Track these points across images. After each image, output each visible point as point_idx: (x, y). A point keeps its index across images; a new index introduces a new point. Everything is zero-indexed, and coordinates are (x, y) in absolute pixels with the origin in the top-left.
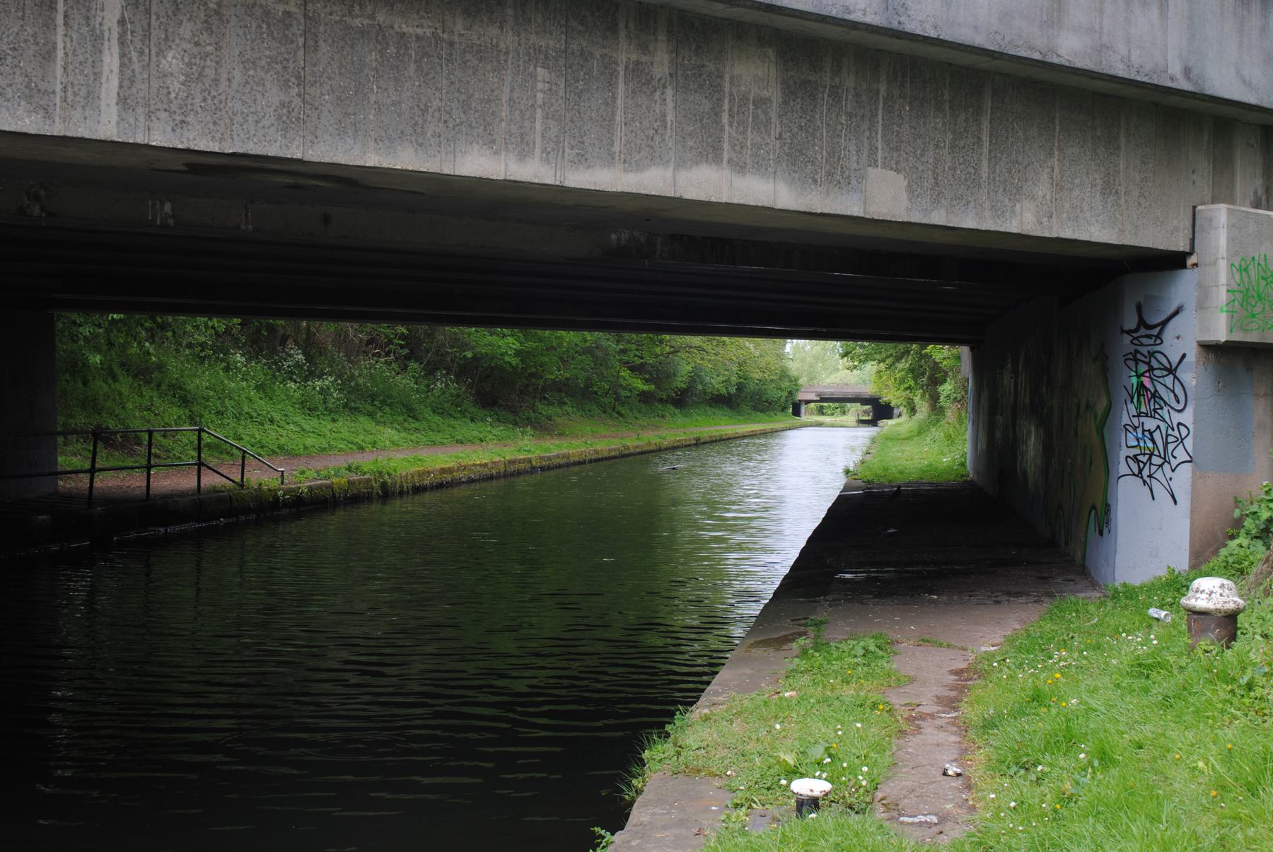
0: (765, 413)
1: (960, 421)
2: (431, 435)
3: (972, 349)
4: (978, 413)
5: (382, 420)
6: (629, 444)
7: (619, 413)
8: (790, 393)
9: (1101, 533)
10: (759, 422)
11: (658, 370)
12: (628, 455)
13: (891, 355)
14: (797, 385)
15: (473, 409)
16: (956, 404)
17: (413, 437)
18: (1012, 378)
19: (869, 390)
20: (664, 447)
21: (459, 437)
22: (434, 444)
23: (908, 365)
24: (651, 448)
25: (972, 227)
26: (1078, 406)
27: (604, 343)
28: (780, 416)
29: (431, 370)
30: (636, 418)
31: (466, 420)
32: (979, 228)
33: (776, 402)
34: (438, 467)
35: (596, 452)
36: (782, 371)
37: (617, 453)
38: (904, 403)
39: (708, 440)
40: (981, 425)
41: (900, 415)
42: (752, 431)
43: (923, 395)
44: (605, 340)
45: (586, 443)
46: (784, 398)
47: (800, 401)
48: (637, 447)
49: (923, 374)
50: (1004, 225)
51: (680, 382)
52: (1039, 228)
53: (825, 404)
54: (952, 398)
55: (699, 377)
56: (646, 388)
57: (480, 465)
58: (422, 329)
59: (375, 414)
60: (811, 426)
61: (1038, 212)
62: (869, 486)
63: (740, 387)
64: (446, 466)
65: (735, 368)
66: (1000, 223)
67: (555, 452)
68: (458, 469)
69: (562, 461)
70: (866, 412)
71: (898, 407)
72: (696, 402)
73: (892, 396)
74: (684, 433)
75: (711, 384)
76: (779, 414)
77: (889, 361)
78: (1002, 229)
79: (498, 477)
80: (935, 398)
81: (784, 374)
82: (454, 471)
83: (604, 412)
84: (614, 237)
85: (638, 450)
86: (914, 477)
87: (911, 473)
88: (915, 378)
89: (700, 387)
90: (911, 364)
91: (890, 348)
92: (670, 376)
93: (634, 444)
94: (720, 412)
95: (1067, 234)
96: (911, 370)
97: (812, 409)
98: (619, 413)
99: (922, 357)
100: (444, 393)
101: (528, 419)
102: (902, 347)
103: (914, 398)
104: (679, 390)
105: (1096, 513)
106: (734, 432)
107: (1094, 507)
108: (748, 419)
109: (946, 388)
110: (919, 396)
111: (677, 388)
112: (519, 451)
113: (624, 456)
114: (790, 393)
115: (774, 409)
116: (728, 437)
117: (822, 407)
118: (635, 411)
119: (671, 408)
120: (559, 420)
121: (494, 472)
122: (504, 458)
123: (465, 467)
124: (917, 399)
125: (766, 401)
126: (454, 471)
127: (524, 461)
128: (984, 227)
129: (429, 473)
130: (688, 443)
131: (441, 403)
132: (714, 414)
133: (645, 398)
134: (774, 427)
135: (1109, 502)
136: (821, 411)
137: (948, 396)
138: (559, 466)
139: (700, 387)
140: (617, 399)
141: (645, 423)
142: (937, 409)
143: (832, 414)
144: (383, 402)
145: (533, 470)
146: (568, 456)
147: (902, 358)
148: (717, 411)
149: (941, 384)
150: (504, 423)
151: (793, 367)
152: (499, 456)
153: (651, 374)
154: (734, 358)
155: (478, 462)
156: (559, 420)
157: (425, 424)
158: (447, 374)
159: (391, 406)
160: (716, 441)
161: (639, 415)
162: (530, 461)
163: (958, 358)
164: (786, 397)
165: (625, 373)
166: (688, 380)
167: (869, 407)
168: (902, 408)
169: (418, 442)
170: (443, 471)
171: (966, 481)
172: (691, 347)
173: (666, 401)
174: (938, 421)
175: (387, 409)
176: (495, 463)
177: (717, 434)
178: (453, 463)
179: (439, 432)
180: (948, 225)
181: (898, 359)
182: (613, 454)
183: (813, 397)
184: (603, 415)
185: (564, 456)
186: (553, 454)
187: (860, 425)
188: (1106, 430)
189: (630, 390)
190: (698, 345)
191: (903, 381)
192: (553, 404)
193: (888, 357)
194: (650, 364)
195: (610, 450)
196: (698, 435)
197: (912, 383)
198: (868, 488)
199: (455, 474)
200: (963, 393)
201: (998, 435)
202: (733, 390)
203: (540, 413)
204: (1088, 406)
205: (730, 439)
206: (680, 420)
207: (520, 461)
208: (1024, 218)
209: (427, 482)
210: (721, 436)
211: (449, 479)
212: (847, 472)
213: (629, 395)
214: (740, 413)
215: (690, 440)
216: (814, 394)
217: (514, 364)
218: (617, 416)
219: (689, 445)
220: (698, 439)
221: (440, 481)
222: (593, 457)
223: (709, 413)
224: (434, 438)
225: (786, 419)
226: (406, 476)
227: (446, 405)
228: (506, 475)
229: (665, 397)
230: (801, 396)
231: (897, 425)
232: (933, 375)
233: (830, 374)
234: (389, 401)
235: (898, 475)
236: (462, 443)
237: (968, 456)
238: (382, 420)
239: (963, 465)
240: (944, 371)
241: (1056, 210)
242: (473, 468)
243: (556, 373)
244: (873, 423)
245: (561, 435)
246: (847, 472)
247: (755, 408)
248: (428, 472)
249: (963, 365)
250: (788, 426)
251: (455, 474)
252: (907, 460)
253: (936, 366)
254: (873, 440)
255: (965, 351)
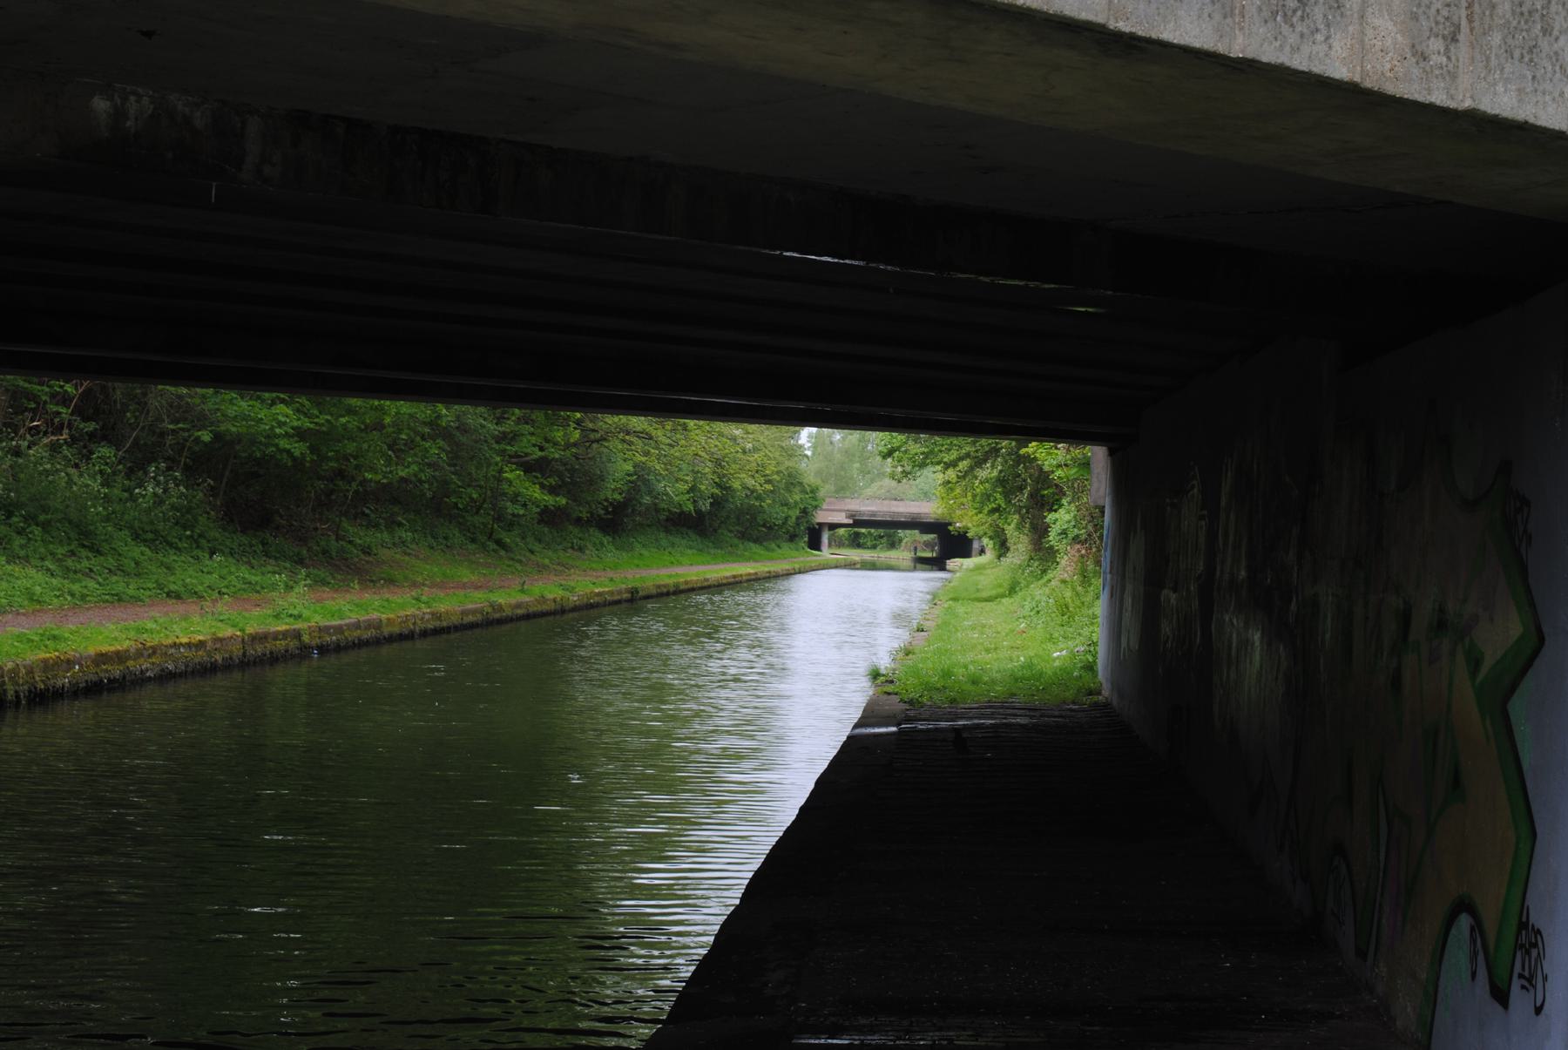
0: (761, 544)
1: (1085, 579)
2: (118, 584)
3: (1112, 453)
4: (1123, 577)
5: (22, 553)
6: (501, 601)
7: (499, 543)
8: (804, 511)
9: (1501, 996)
10: (748, 560)
11: (572, 471)
12: (500, 622)
13: (968, 455)
14: (815, 499)
15: (215, 534)
16: (1078, 546)
17: (76, 587)
18: (1202, 518)
19: (931, 509)
20: (571, 605)
21: (173, 587)
22: (120, 600)
23: (995, 473)
24: (545, 608)
25: (1197, 44)
26: (1405, 619)
27: (471, 420)
28: (786, 549)
29: (136, 464)
30: (532, 552)
31: (200, 553)
32: (1221, 48)
33: (781, 527)
34: (92, 651)
35: (436, 616)
36: (790, 475)
37: (479, 617)
38: (990, 533)
39: (654, 592)
40: (1128, 601)
41: (982, 551)
42: (734, 577)
43: (1019, 527)
44: (478, 418)
45: (417, 599)
46: (794, 519)
47: (820, 524)
48: (518, 606)
49: (1021, 489)
50: (1306, 49)
51: (612, 490)
52: (1416, 72)
53: (863, 530)
54: (1070, 536)
55: (646, 482)
56: (549, 500)
57: (189, 645)
58: (119, 390)
59: (10, 541)
60: (836, 567)
61: (1415, 17)
62: (912, 713)
63: (717, 503)
64: (112, 649)
65: (707, 469)
66: (1293, 39)
67: (353, 617)
68: (139, 654)
69: (367, 635)
70: (928, 545)
71: (980, 538)
72: (641, 525)
73: (968, 521)
74: (611, 580)
75: (667, 494)
76: (785, 545)
77: (963, 465)
78: (1299, 63)
79: (228, 666)
80: (1040, 532)
81: (793, 480)
82: (128, 658)
83: (473, 541)
84: (100, 105)
85: (520, 612)
86: (992, 707)
87: (993, 682)
88: (1007, 495)
89: (647, 500)
90: (1001, 471)
91: (962, 446)
92: (595, 480)
93: (513, 601)
94: (684, 542)
95: (1503, 102)
96: (1001, 481)
97: (841, 538)
98: (499, 543)
99: (1021, 460)
100: (161, 502)
101: (325, 552)
102: (985, 443)
103: (1006, 527)
104: (611, 504)
105: (1477, 927)
106: (701, 578)
107: (1464, 906)
108: (730, 553)
109: (1062, 518)
110: (1013, 526)
111: (606, 500)
112: (277, 616)
113: (492, 623)
114: (804, 511)
115: (776, 538)
116: (690, 586)
117: (857, 535)
118: (530, 539)
119: (596, 535)
120: (385, 554)
121: (218, 657)
122: (242, 630)
123: (154, 650)
124: (1010, 530)
125: (764, 526)
126: (128, 658)
127: (285, 634)
128: (1238, 46)
129: (69, 663)
130: (617, 598)
131: (152, 523)
132: (673, 545)
133: (550, 517)
134: (772, 569)
135: (1536, 919)
136: (855, 541)
137: (1064, 533)
138: (361, 644)
139: (647, 500)
140: (499, 518)
141: (547, 561)
142: (1043, 554)
143: (874, 547)
144: (30, 519)
145: (304, 652)
146: (378, 625)
147: (985, 461)
148: (677, 540)
149: (1051, 510)
150: (276, 559)
151: (809, 472)
152: (233, 626)
153: (561, 476)
154: (703, 454)
155: (184, 640)
156: (385, 554)
157: (111, 562)
158: (169, 469)
159: (46, 526)
160: (668, 594)
161: (537, 547)
162: (297, 635)
163: (1086, 465)
164: (798, 518)
165: (513, 474)
166: (625, 488)
167: (932, 536)
168: (985, 541)
169: (83, 597)
170: (102, 658)
171: (1096, 705)
172: (628, 433)
173: (589, 522)
174: (1044, 572)
175: (37, 531)
176: (221, 640)
177: (670, 581)
178: (126, 644)
179: (138, 575)
180: (1112, 25)
181: (979, 463)
182: (471, 618)
183: (841, 518)
184: (472, 547)
185: (370, 625)
186: (347, 621)
187: (918, 566)
188: (1517, 707)
189: (525, 505)
190: (638, 429)
191: (987, 497)
192: (376, 526)
193: (961, 459)
194: (557, 460)
195: (464, 613)
196: (638, 584)
197: (1001, 502)
198: (908, 720)
199: (130, 663)
200: (1090, 528)
201: (1166, 628)
202: (705, 506)
203: (350, 542)
204: (1441, 625)
205: (693, 590)
206: (611, 555)
207: (276, 636)
208: (1370, 33)
209: (64, 681)
210: (676, 585)
211: (117, 674)
212: (875, 675)
213: (521, 512)
214: (718, 544)
215: (620, 592)
216: (844, 514)
217: (297, 453)
218: (495, 547)
219: (618, 602)
220: (634, 591)
221: (95, 678)
222: (430, 626)
223: (664, 542)
224: (120, 587)
225: (794, 553)
226: (16, 670)
227: (161, 526)
228: (245, 664)
229: (585, 515)
230: (822, 517)
231: (979, 569)
232: (1038, 490)
233: (872, 481)
234: (42, 518)
235: (969, 687)
236: (178, 597)
237: (1102, 651)
238: (22, 553)
239: (1090, 668)
240: (1057, 486)
241: (1470, 19)
242: (173, 651)
243: (379, 471)
244: (938, 564)
245: (391, 581)
246: (875, 675)
247: (744, 536)
248: (68, 661)
249: (1095, 479)
250: (797, 566)
251: (130, 663)
252: (988, 651)
253: (1043, 478)
254: (934, 599)
255: (1097, 454)
